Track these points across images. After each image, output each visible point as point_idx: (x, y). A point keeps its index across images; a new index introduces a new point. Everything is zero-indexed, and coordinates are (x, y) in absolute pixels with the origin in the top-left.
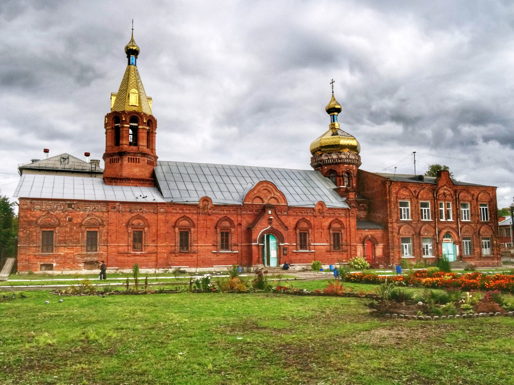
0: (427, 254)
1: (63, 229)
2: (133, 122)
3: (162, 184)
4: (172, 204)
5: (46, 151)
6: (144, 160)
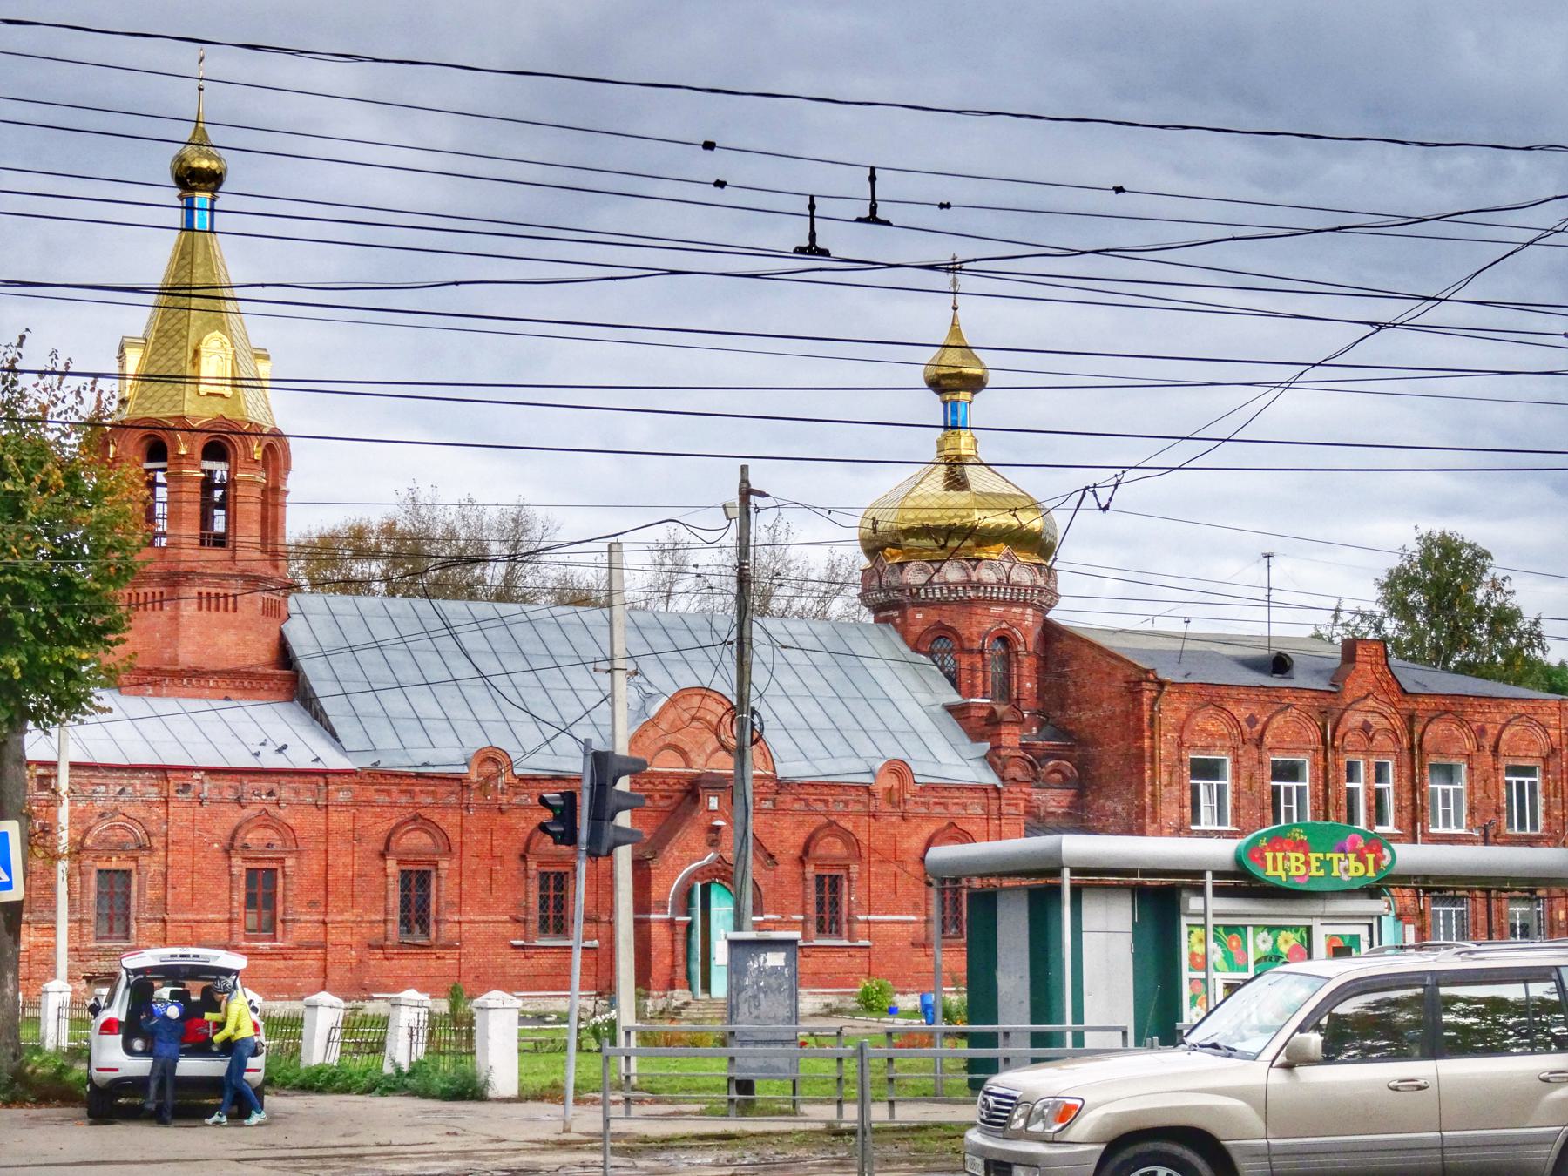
4: (378, 775)
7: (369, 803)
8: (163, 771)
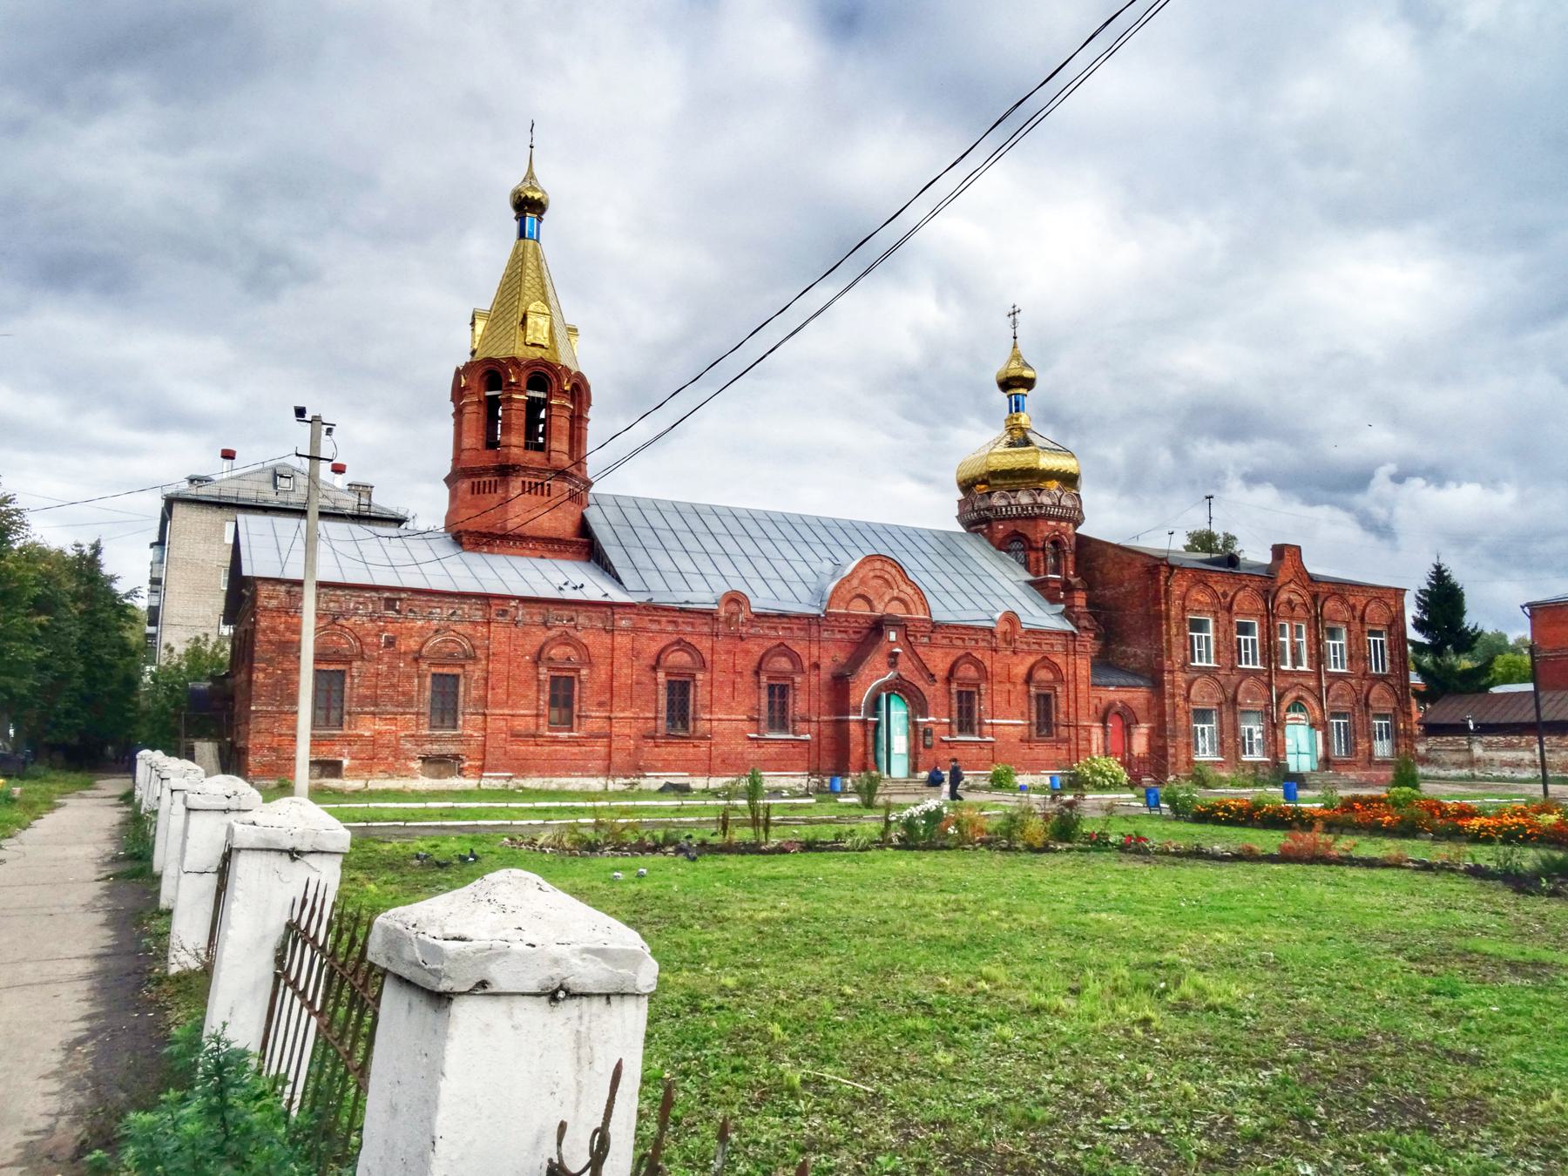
0: (1251, 752)
1: (371, 668)
2: (533, 389)
3: (614, 555)
4: (651, 609)
5: (228, 455)
6: (560, 487)
7: (645, 630)
8: (486, 598)
